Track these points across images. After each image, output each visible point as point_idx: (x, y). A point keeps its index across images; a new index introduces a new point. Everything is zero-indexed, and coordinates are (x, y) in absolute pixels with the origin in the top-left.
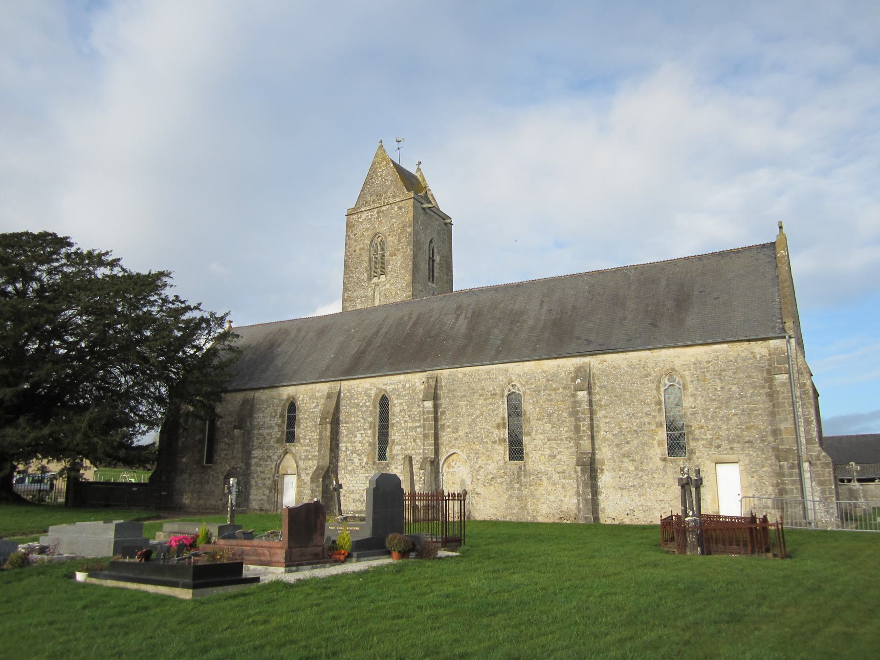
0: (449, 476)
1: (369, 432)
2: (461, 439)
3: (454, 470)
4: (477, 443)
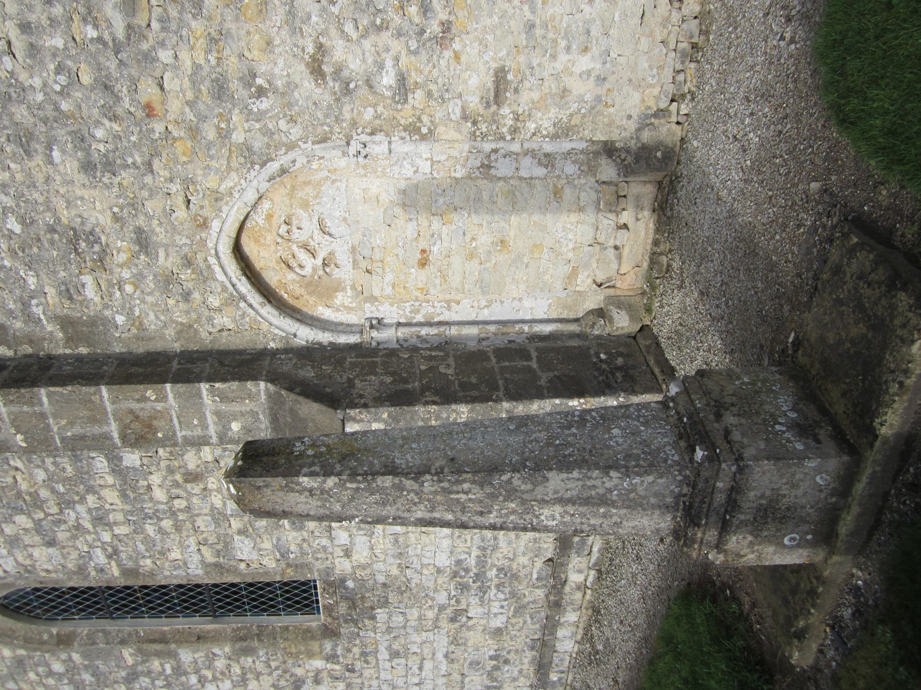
0: (379, 286)
1: (186, 656)
2: (135, 205)
3: (343, 257)
4: (148, 91)
